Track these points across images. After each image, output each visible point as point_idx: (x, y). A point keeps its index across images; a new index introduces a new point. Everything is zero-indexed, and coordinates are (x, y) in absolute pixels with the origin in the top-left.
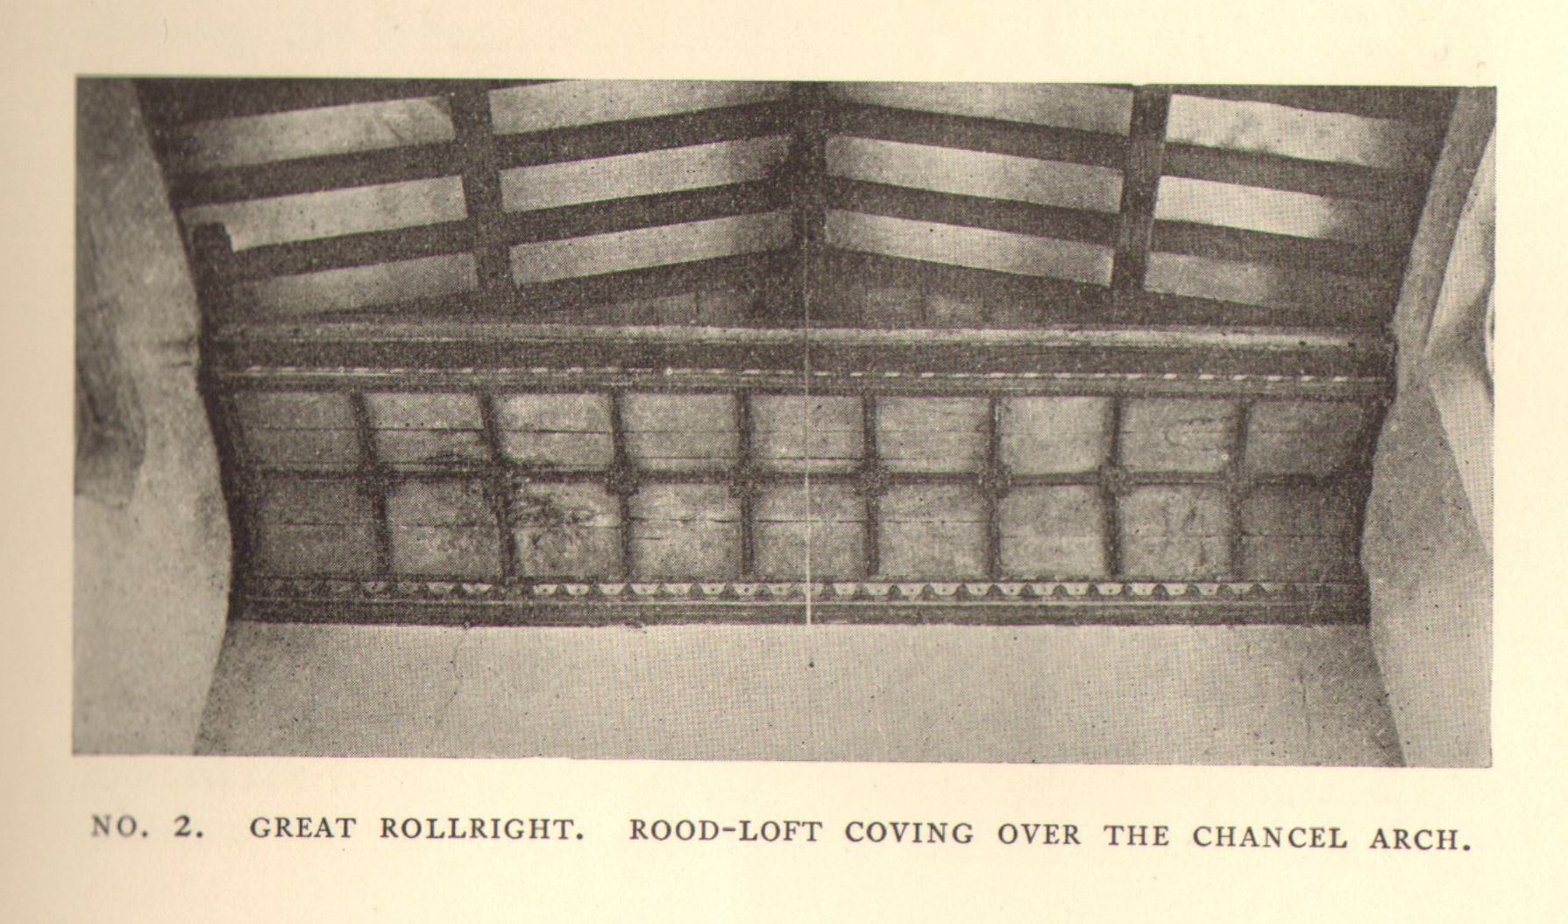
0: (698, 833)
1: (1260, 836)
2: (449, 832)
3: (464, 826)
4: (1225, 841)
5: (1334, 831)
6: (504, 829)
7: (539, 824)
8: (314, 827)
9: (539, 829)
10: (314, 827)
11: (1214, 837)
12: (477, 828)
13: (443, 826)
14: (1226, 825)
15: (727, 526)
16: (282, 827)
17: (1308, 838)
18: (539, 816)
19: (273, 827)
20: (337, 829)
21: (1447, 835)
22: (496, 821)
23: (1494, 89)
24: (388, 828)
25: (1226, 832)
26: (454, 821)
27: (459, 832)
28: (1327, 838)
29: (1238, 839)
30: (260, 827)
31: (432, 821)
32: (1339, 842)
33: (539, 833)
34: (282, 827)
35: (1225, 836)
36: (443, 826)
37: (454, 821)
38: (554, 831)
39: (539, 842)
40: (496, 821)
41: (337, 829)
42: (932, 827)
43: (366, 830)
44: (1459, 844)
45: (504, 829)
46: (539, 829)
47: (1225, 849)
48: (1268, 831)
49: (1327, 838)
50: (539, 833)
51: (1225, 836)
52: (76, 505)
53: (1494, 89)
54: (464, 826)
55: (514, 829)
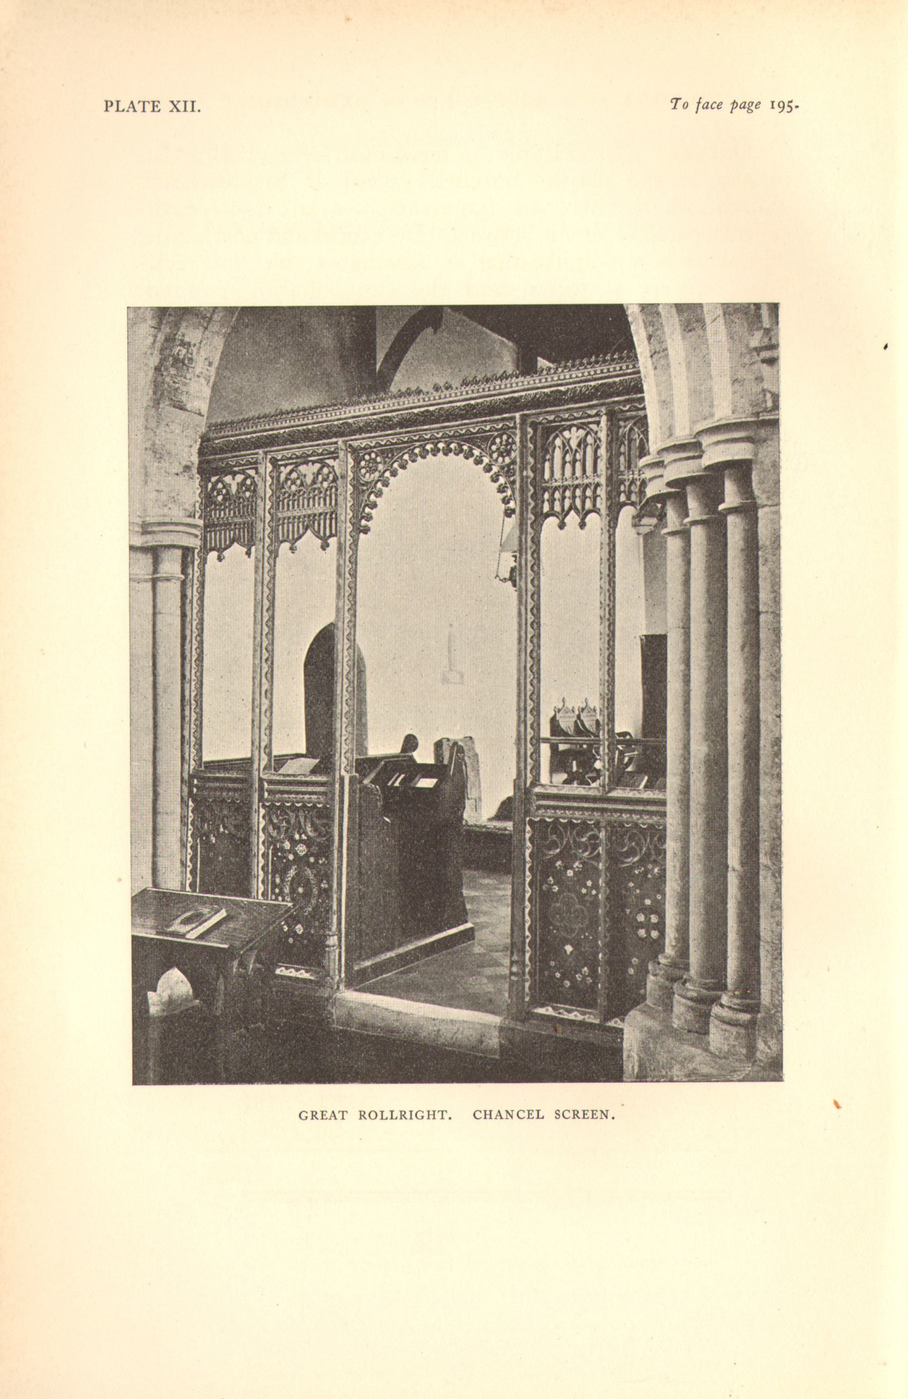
0: (414, 1114)
1: (504, 1115)
2: (390, 1117)
3: (397, 1114)
4: (488, 1117)
5: (538, 1111)
6: (415, 1115)
7: (431, 1113)
8: (328, 1115)
9: (431, 1115)
10: (328, 1115)
11: (483, 1115)
12: (403, 1115)
13: (387, 1114)
14: (488, 1109)
15: (515, 951)
16: (314, 1115)
17: (526, 1115)
18: (431, 1109)
19: (310, 1115)
20: (339, 1116)
21: (488, 1113)
22: (411, 1112)
23: (140, 1078)
24: (362, 1115)
25: (488, 1113)
26: (392, 1112)
27: (394, 1117)
28: (535, 1115)
29: (494, 1115)
30: (303, 1116)
31: (382, 1112)
32: (541, 1116)
33: (431, 1117)
34: (314, 1115)
35: (488, 1114)
36: (387, 1114)
37: (392, 1112)
38: (438, 1116)
39: (431, 1120)
40: (411, 1112)
41: (339, 1116)
42: (602, 1112)
43: (353, 1115)
44: (610, 1117)
45: (415, 1115)
46: (431, 1115)
47: (488, 1120)
48: (507, 1112)
49: (535, 1114)
50: (431, 1117)
51: (488, 1114)
52: (779, 388)
53: (140, 1078)
54: (397, 1114)
55: (419, 1115)
